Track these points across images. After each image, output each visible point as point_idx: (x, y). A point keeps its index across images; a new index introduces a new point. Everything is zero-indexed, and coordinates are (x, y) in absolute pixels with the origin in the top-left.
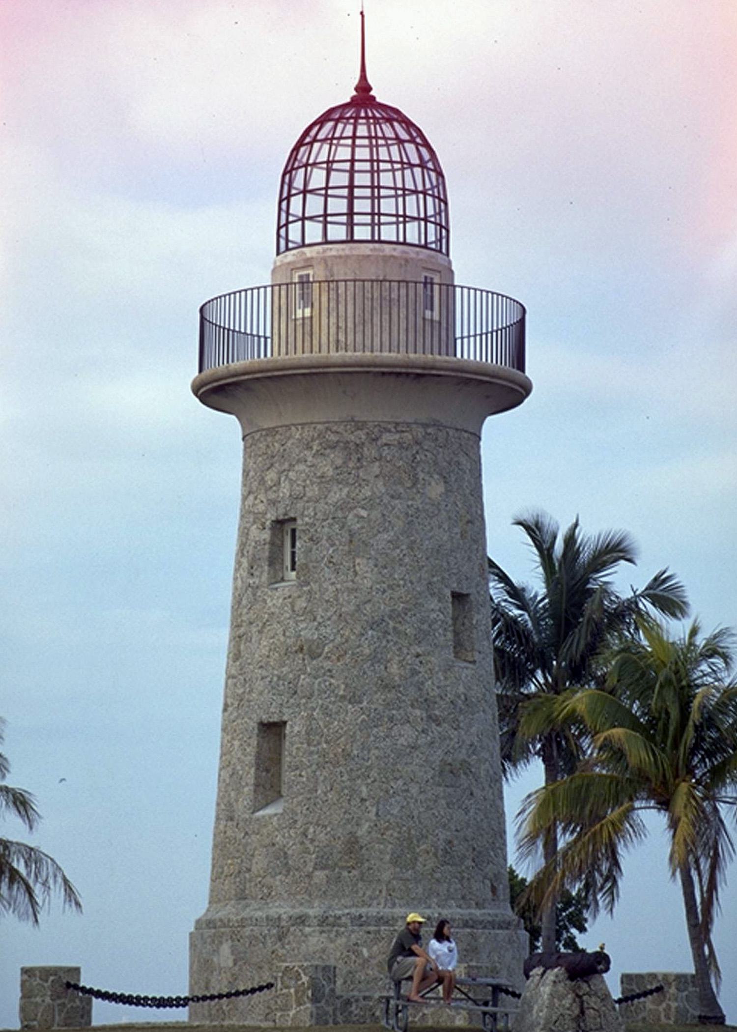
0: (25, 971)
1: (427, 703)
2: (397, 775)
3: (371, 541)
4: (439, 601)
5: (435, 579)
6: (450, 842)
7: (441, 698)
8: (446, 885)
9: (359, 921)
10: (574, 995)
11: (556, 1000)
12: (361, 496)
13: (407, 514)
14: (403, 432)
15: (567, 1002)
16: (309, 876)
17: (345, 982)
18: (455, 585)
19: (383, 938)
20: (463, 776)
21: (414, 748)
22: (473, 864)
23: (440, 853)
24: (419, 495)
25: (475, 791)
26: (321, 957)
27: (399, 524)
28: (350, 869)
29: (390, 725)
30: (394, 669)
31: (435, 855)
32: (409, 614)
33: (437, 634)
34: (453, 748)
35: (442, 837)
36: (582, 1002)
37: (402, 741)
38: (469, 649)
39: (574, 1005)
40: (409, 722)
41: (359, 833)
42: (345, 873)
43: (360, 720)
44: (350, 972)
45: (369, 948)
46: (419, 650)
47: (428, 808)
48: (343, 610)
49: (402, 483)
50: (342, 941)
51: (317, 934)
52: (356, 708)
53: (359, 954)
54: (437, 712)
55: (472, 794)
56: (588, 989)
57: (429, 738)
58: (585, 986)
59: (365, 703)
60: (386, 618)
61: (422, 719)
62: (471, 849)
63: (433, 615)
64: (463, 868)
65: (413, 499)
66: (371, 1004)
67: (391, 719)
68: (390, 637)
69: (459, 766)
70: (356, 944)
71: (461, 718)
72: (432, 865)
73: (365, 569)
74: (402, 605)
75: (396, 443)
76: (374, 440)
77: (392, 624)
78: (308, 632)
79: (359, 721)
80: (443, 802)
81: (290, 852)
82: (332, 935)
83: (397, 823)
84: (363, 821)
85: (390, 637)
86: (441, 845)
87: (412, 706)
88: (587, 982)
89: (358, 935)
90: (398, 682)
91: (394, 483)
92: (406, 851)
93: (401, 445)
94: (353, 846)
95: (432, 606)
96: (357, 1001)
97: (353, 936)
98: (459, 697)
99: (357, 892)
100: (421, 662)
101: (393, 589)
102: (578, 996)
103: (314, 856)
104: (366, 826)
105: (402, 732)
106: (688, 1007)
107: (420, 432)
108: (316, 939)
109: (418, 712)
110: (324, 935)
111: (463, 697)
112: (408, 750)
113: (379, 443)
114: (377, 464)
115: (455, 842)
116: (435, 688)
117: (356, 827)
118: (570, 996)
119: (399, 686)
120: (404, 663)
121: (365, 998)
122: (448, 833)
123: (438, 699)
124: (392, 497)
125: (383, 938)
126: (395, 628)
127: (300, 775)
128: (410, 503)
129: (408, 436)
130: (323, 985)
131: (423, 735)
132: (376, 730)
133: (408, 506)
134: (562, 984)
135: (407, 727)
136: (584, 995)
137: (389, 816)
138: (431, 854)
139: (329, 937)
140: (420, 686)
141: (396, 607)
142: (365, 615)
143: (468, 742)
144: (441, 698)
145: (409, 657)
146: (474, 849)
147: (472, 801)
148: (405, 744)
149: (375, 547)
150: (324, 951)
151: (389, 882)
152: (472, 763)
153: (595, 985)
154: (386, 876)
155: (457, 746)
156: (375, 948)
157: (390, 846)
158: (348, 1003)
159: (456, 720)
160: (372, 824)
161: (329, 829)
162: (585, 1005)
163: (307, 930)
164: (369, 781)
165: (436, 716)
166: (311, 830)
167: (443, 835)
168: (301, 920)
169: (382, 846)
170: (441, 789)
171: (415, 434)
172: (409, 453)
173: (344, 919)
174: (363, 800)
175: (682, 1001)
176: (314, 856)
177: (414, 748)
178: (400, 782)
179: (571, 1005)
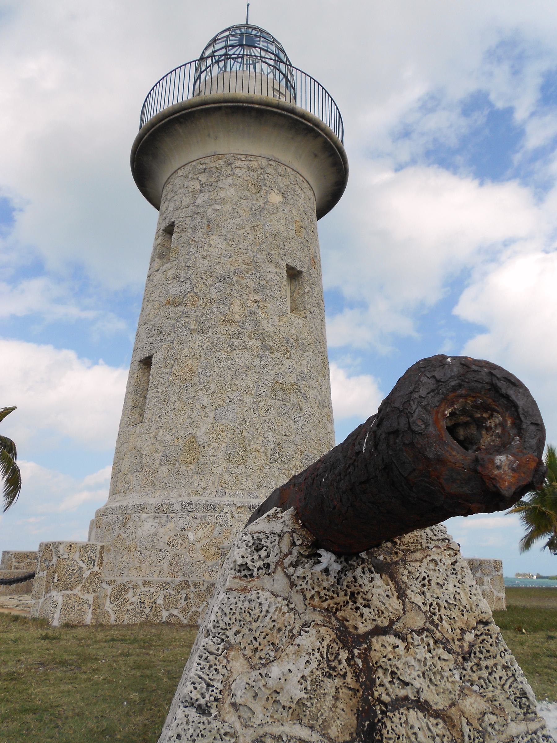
0: (5, 553)
1: (263, 336)
2: (234, 388)
3: (223, 224)
4: (276, 267)
5: (273, 252)
6: (279, 444)
7: (275, 334)
8: (274, 479)
9: (189, 508)
10: (329, 635)
11: (238, 665)
12: (218, 197)
13: (251, 209)
14: (250, 161)
15: (291, 672)
16: (156, 471)
17: (171, 564)
18: (290, 261)
19: (209, 524)
20: (292, 394)
21: (250, 368)
22: (301, 465)
23: (269, 452)
24: (262, 199)
25: (303, 406)
26: (153, 541)
27: (244, 215)
28: (188, 464)
29: (229, 350)
30: (236, 309)
31: (265, 453)
32: (250, 272)
33: (273, 289)
34: (285, 372)
35: (271, 439)
36: (366, 675)
37: (240, 362)
38: (302, 309)
39: (329, 685)
40: (247, 348)
41: (198, 434)
42: (184, 467)
43: (205, 346)
44: (177, 555)
45: (196, 532)
46: (257, 298)
47: (259, 415)
48: (199, 270)
49: (249, 190)
50: (171, 525)
51: (151, 519)
52: (203, 337)
53: (185, 538)
54: (271, 343)
55: (301, 409)
56: (395, 604)
57: (263, 362)
58: (378, 588)
59: (210, 334)
60: (231, 274)
61: (257, 347)
62: (299, 453)
63: (270, 276)
64: (291, 466)
65: (257, 200)
66: (152, 590)
67: (231, 345)
68: (234, 287)
69: (289, 386)
70: (183, 529)
71: (293, 351)
72: (263, 462)
73: (217, 242)
74: (243, 265)
75: (245, 167)
76: (229, 164)
77: (235, 278)
78: (173, 289)
79: (204, 347)
80: (274, 411)
81: (144, 453)
82: (163, 520)
83: (231, 426)
84: (201, 424)
85: (234, 287)
86: (271, 445)
87: (250, 337)
88: (387, 570)
89: (185, 520)
90: (239, 319)
91: (244, 190)
92: (238, 449)
93: (249, 169)
94: (193, 444)
95: (270, 270)
96: (135, 586)
97: (181, 521)
98: (291, 336)
99: (192, 483)
100: (259, 306)
101: (237, 255)
102: (347, 638)
103: (161, 454)
104: (204, 429)
105: (240, 356)
106: (493, 590)
107: (264, 162)
108: (150, 524)
109: (254, 342)
110: (156, 521)
111: (294, 337)
112: (244, 370)
113: (233, 166)
114: (231, 178)
115: (284, 445)
116: (270, 326)
117: (195, 429)
118: (307, 641)
119: (239, 322)
120: (244, 306)
121: (145, 583)
122: (278, 437)
123: (272, 334)
124: (241, 198)
125: (209, 524)
126: (237, 281)
127: (157, 392)
128: (254, 202)
129: (255, 164)
130: (80, 568)
131: (258, 359)
132: (217, 353)
133: (253, 204)
134: (279, 582)
135: (244, 352)
136: (379, 631)
137: (224, 420)
138: (261, 453)
139: (160, 523)
140: (257, 324)
141: (240, 267)
142: (215, 272)
143: (299, 370)
144: (275, 334)
145: (248, 302)
146: (302, 453)
147: (301, 415)
148: (242, 364)
149: (226, 228)
150: (155, 535)
151: (222, 475)
152: (301, 386)
153: (425, 582)
154: (219, 470)
155: (288, 370)
156: (200, 533)
157: (224, 445)
158: (123, 588)
159: (287, 351)
160: (209, 426)
161: (174, 432)
162: (387, 690)
163: (144, 516)
164: (209, 392)
165: (270, 346)
166: (161, 433)
167: (272, 438)
168: (141, 508)
169: (216, 445)
170: (273, 401)
171: (260, 162)
172: (255, 174)
173: (175, 507)
174: (203, 407)
175: (488, 585)
176: (161, 454)
177: (250, 368)
178: (236, 394)
179: (314, 686)
